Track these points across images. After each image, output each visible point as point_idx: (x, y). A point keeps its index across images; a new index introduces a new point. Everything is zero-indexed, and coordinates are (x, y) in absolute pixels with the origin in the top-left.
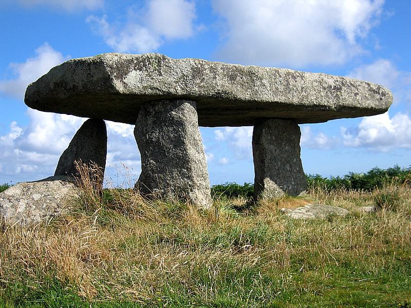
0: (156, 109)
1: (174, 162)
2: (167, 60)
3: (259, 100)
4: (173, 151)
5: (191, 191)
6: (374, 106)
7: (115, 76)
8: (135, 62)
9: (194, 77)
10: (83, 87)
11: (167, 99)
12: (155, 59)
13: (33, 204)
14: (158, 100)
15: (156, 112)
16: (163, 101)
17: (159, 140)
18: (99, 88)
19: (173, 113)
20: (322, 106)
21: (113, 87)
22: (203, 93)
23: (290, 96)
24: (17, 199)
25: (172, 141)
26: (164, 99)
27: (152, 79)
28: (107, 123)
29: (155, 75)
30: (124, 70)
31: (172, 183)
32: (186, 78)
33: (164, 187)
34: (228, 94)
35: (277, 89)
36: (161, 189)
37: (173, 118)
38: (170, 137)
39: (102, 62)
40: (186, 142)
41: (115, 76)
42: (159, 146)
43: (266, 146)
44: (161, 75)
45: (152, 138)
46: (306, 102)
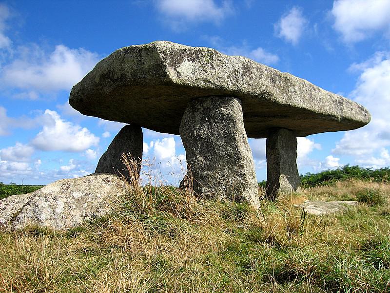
0: (205, 105)
1: (225, 159)
2: (219, 54)
3: (293, 105)
4: (222, 148)
5: (244, 190)
6: (362, 120)
7: (168, 64)
8: (188, 53)
9: (244, 73)
10: (132, 76)
11: (216, 96)
12: (207, 52)
13: (73, 203)
14: (207, 96)
15: (204, 109)
16: (212, 97)
17: (208, 136)
18: (149, 77)
19: (223, 109)
20: (333, 116)
21: (165, 75)
22: (251, 91)
23: (313, 105)
24: (55, 198)
25: (222, 138)
26: (212, 96)
27: (205, 71)
28: (143, 129)
29: (208, 67)
30: (177, 58)
31: (223, 182)
32: (237, 74)
33: (214, 185)
34: (270, 95)
35: (305, 97)
36: (211, 188)
37: (223, 115)
38: (219, 134)
39: (155, 48)
40: (237, 138)
41: (168, 64)
42: (208, 142)
43: (280, 151)
44: (213, 68)
45: (201, 135)
46: (323, 111)
